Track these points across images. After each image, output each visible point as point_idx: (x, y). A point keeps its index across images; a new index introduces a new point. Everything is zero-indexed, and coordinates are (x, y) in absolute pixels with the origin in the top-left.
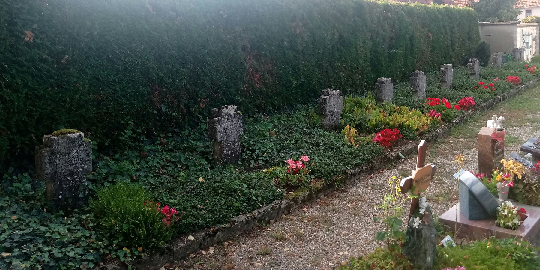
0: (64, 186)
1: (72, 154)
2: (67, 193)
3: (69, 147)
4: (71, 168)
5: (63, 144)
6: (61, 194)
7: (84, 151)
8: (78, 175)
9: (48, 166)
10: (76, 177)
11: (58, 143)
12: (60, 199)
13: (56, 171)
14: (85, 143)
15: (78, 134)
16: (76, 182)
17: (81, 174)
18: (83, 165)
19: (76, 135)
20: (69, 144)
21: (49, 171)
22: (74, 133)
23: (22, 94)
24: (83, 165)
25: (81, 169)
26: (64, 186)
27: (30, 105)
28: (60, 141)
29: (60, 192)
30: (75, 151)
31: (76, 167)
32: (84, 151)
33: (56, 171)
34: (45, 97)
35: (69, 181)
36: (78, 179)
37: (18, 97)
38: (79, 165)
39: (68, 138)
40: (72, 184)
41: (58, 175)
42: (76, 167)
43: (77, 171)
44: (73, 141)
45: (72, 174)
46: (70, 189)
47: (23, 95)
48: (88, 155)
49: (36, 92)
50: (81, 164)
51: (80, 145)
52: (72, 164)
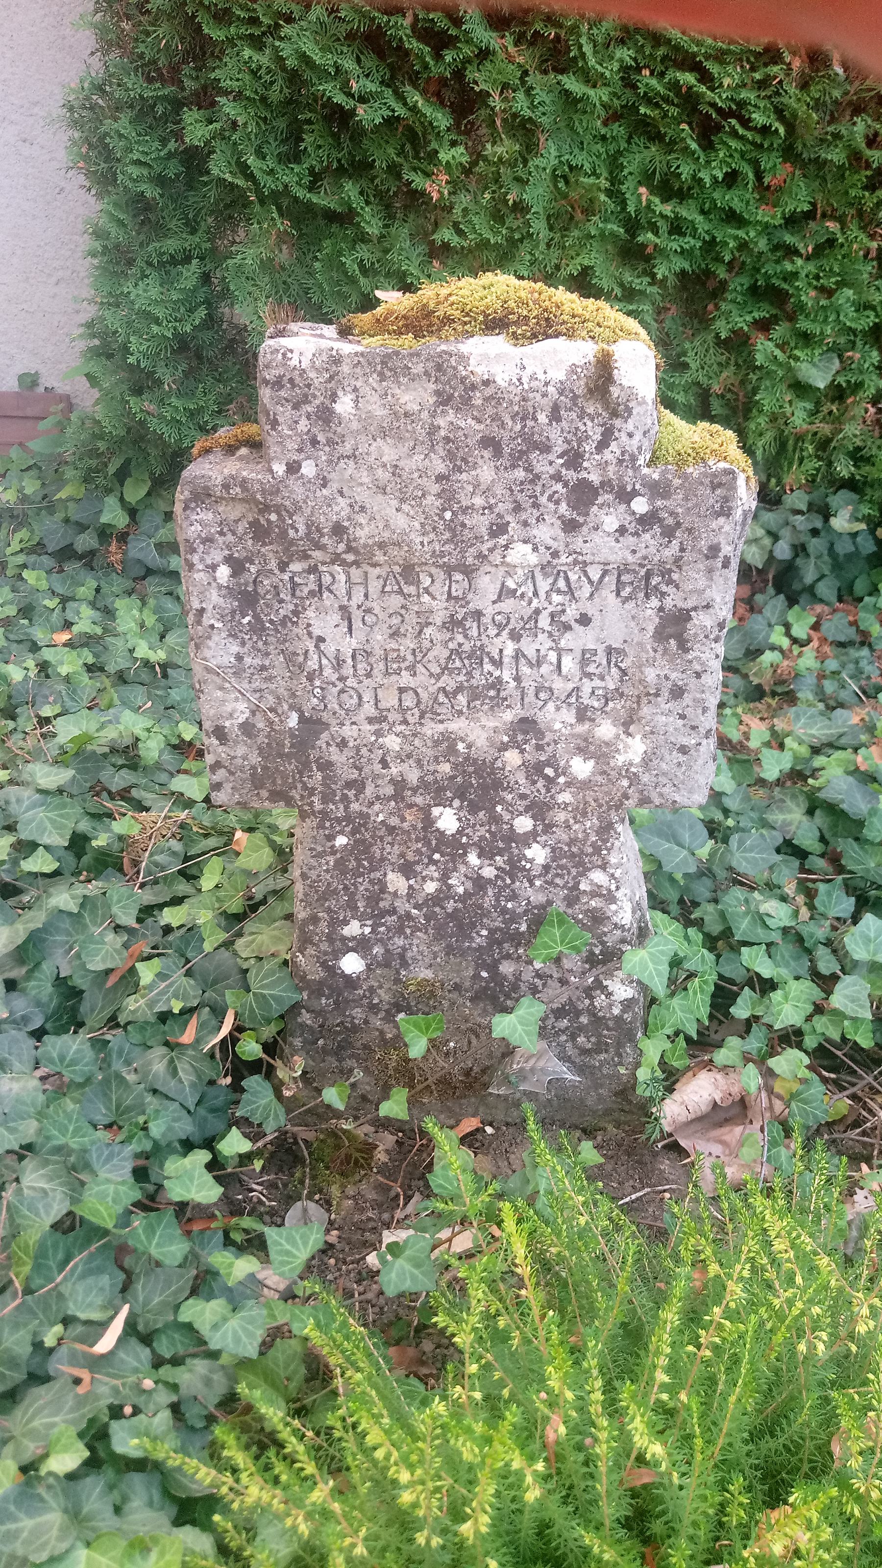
0: (396, 882)
1: (487, 584)
2: (419, 945)
3: (448, 497)
4: (478, 732)
5: (389, 451)
6: (361, 945)
7: (645, 580)
8: (539, 810)
9: (221, 651)
10: (524, 824)
11: (326, 416)
12: (351, 982)
13: (312, 725)
14: (658, 490)
15: (578, 352)
16: (515, 868)
17: (581, 812)
18: (606, 730)
19: (558, 360)
20: (459, 461)
21: (241, 711)
22: (546, 327)
23: (590, 79)
24: (606, 730)
25: (581, 768)
26: (396, 882)
27: (647, 178)
28: (344, 406)
29: (353, 929)
30: (521, 554)
31: (527, 726)
32: (645, 580)
33: (312, 725)
34: (745, 123)
35: (453, 848)
36: (538, 854)
37: (569, 100)
38: (558, 719)
39: (457, 390)
40: (480, 883)
41: (326, 766)
42: (527, 726)
43: (535, 770)
44: (512, 434)
45: (478, 786)
46: (452, 923)
47: (599, 95)
48: (674, 627)
49: (688, 78)
50: (583, 714)
51: (583, 495)
52: (492, 694)
